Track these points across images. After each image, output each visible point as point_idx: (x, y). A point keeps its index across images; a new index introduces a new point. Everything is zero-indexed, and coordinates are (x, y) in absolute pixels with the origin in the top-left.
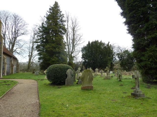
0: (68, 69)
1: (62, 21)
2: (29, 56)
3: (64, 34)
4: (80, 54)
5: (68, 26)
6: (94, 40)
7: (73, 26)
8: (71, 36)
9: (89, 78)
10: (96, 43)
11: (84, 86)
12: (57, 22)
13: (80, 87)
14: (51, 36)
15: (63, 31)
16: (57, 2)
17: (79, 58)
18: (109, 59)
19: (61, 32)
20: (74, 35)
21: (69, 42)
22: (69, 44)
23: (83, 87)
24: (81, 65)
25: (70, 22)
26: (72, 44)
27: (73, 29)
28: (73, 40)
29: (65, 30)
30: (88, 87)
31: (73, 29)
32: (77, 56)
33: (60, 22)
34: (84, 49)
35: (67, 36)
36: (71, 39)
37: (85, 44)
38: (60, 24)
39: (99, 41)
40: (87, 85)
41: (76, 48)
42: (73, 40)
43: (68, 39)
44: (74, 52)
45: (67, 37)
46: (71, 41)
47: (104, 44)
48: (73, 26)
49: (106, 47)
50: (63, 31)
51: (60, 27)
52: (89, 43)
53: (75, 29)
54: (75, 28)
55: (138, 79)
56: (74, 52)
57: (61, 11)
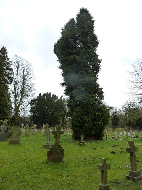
0: (2, 125)
1: (9, 68)
2: (14, 95)
3: (9, 83)
4: (29, 107)
5: (16, 73)
6: (46, 93)
7: (24, 74)
8: (20, 85)
9: (17, 133)
10: (48, 95)
11: (11, 140)
12: (3, 69)
13: (6, 143)
14: (83, 55)
15: (8, 80)
16: (5, 47)
17: (27, 111)
18: (61, 115)
19: (6, 81)
20: (24, 84)
21: (18, 92)
22: (17, 95)
23: (11, 141)
24: (30, 120)
25: (20, 71)
26: (20, 94)
27: (24, 78)
28: (23, 90)
29: (12, 80)
30: (15, 141)
31: (24, 78)
32: (26, 109)
33: (6, 70)
34: (34, 101)
35: (15, 85)
36: (19, 88)
37: (36, 95)
38: (6, 72)
39: (52, 94)
40: (14, 140)
41: (25, 100)
42: (23, 90)
43: (17, 89)
44: (22, 104)
45: (14, 86)
46: (19, 91)
47: (56, 97)
48: (24, 74)
49: (58, 101)
50: (8, 80)
51: (6, 76)
52: (40, 94)
53: (26, 78)
54: (26, 76)
55: (49, 134)
56: (21, 104)
57: (8, 57)
